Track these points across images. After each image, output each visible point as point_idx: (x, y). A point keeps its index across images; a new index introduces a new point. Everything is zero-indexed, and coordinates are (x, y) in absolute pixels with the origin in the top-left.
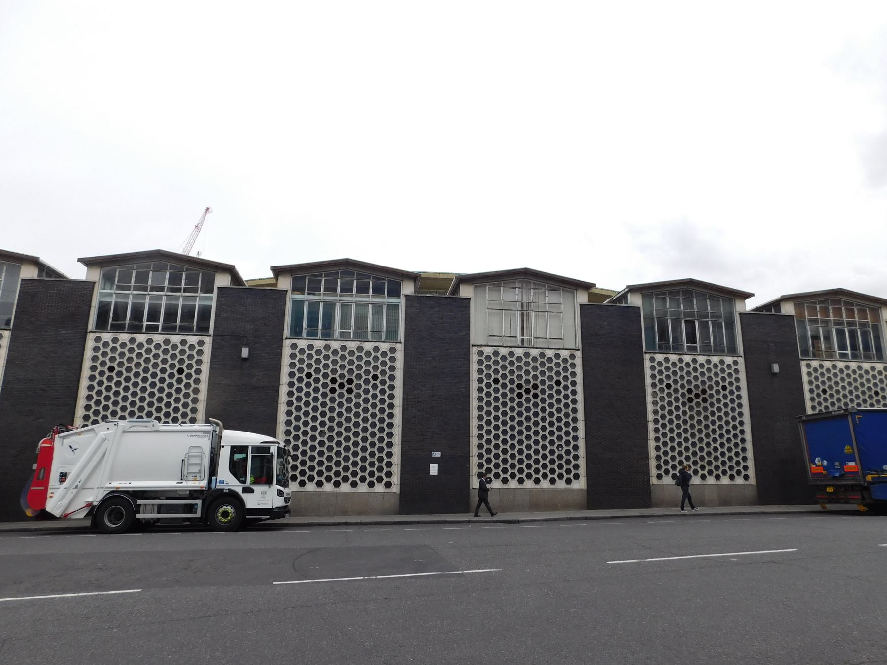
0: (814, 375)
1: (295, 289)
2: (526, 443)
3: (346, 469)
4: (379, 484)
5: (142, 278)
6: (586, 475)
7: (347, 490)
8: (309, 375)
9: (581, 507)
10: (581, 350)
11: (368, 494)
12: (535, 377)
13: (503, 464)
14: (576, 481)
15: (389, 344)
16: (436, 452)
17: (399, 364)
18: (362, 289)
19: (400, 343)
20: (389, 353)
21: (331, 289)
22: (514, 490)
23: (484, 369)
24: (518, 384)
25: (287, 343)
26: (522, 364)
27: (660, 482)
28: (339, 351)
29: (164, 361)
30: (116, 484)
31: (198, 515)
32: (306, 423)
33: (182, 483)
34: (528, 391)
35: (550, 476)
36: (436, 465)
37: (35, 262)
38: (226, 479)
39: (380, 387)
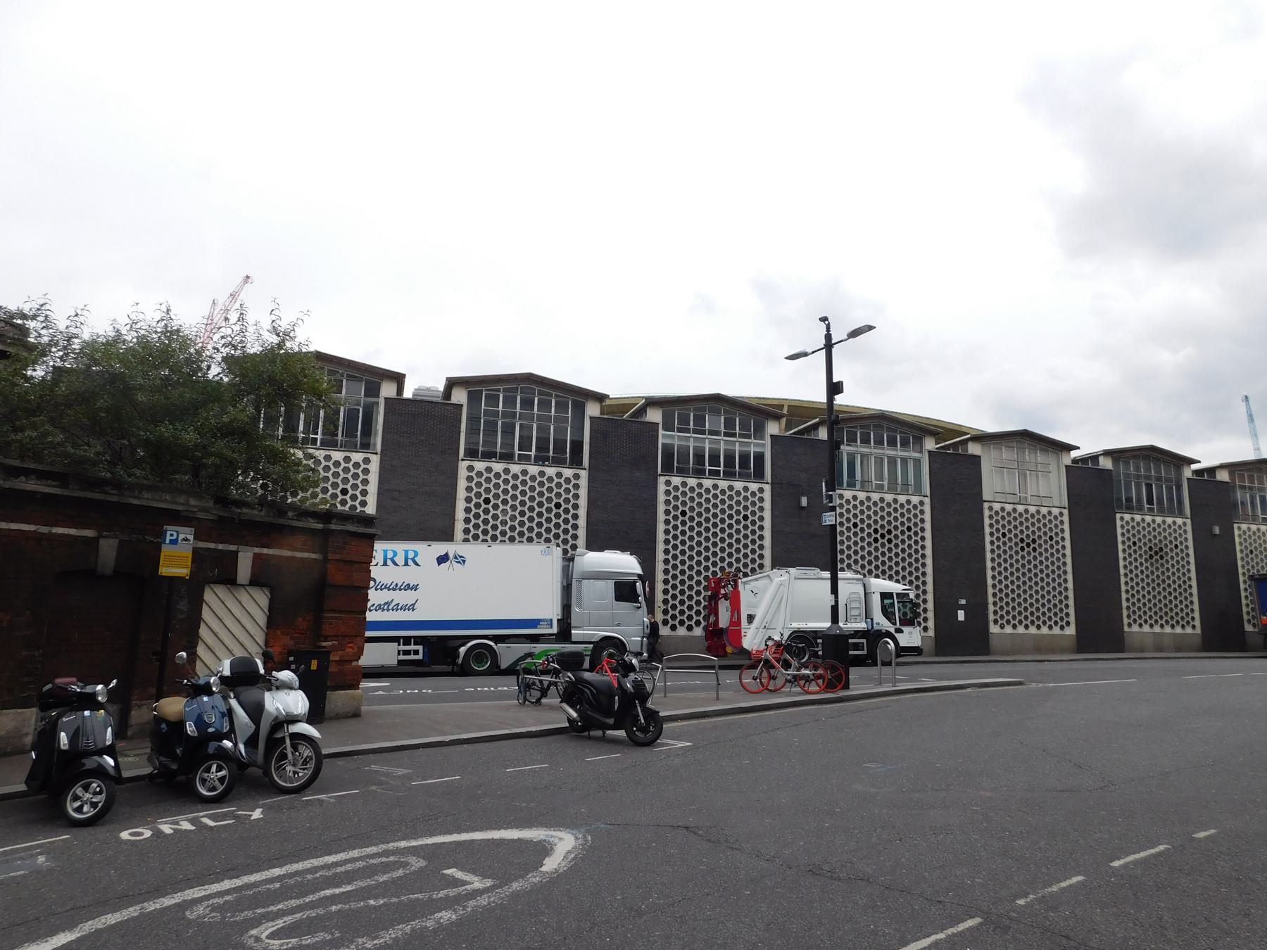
0: (1126, 528)
1: (668, 426)
5: (700, 420)
8: (487, 501)
9: (931, 655)
10: (587, 469)
15: (742, 483)
19: (585, 469)
23: (492, 488)
25: (463, 465)
29: (541, 494)
30: (796, 625)
31: (865, 652)
34: (883, 536)
36: (963, 612)
38: (882, 623)
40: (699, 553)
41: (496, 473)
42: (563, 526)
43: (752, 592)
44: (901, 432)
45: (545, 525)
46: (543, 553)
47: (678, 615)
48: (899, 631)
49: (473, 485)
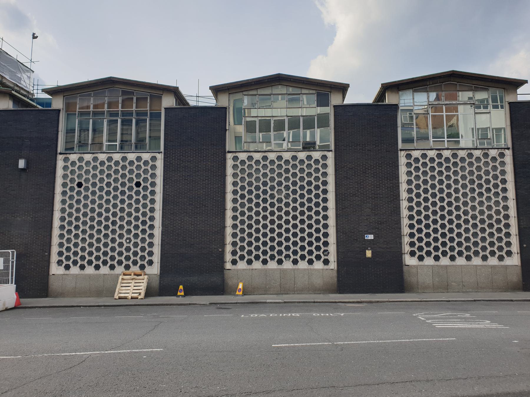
2: (432, 227)
7: (92, 273)
10: (333, 151)
13: (294, 246)
14: (509, 258)
16: (369, 235)
20: (306, 160)
26: (420, 165)
27: (234, 267)
40: (295, 235)
41: (415, 158)
42: (270, 218)
45: (285, 226)
49: (412, 169)
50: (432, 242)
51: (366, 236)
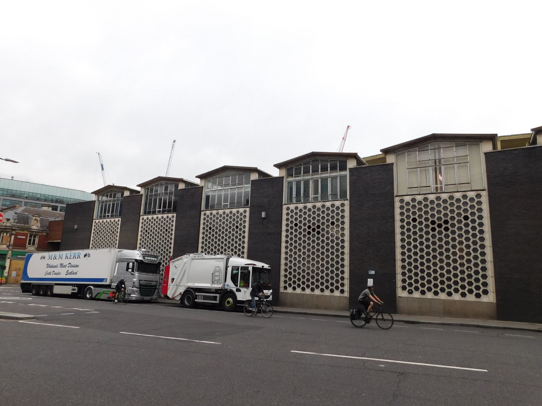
3: (317, 280)
4: (337, 291)
6: (495, 291)
9: (491, 318)
11: (331, 297)
12: (446, 215)
14: (485, 296)
17: (347, 214)
18: (324, 169)
21: (306, 172)
22: (321, 296)
24: (432, 221)
25: (285, 207)
28: (448, 200)
31: (218, 302)
32: (332, 253)
33: (212, 285)
34: (440, 226)
35: (321, 287)
36: (372, 280)
37: (255, 170)
39: (418, 227)
41: (313, 207)
43: (175, 267)
44: (331, 161)
46: (109, 252)
47: (310, 285)
48: (238, 290)
49: (404, 211)
50: (432, 280)
51: (370, 272)
